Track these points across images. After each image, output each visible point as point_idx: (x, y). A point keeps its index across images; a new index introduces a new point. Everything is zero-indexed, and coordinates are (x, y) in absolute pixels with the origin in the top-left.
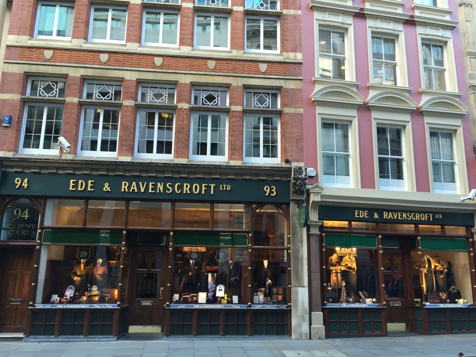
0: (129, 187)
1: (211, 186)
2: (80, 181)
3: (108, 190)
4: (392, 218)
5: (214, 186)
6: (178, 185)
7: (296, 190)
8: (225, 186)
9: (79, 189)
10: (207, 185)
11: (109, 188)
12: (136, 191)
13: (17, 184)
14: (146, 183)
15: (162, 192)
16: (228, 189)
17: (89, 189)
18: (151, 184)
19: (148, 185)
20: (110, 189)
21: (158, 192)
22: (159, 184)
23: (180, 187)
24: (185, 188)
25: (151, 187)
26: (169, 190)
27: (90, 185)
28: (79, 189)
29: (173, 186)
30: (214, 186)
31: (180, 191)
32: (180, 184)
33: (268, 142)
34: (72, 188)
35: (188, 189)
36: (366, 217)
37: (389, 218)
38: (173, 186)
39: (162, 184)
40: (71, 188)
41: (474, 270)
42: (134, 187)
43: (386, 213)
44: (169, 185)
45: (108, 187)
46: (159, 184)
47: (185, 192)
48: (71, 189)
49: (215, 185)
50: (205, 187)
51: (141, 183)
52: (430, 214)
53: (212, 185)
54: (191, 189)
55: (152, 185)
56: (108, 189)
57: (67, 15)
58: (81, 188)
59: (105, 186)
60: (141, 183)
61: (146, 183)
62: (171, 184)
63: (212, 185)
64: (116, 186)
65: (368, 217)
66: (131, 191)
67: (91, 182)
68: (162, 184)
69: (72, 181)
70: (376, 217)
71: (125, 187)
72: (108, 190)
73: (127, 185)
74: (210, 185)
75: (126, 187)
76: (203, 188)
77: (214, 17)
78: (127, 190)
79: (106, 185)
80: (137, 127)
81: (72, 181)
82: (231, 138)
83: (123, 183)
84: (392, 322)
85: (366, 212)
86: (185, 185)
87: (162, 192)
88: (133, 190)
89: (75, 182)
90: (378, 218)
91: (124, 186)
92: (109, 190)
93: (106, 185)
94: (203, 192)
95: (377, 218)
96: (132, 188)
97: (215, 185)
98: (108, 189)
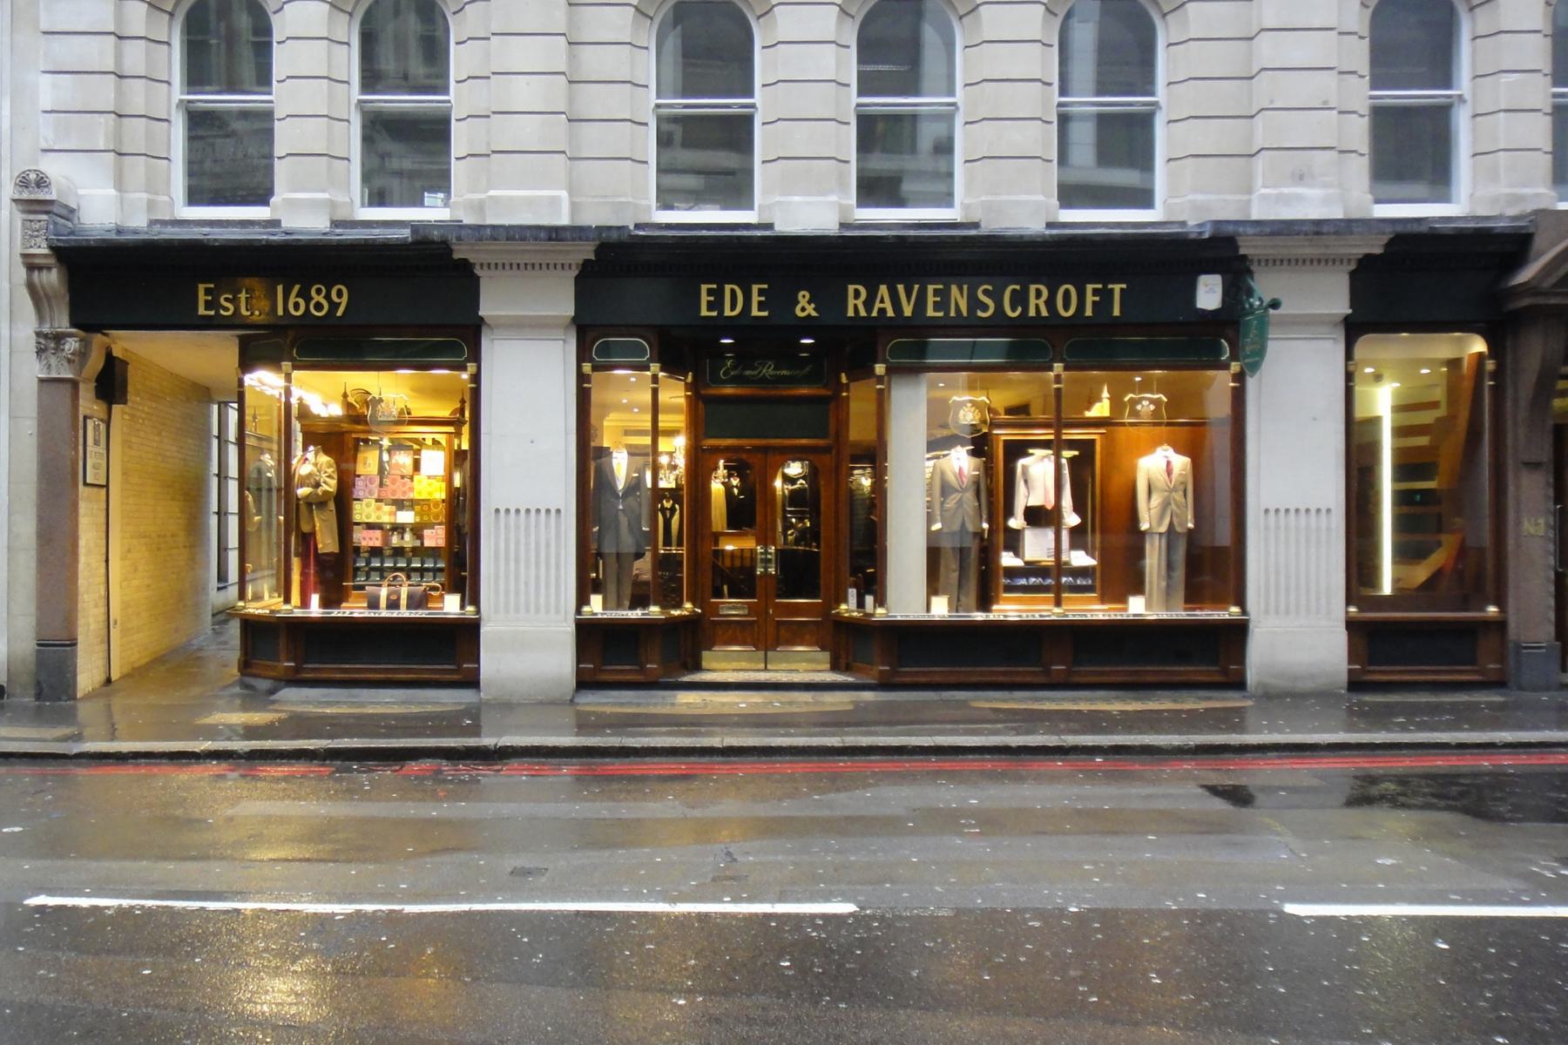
0: (869, 304)
2: (728, 288)
4: (890, 313)
5: (1122, 290)
6: (1014, 291)
9: (728, 313)
10: (1100, 286)
11: (813, 306)
13: (297, 296)
14: (916, 287)
15: (965, 313)
18: (931, 288)
20: (814, 309)
22: (954, 289)
23: (1020, 299)
24: (1033, 301)
25: (931, 299)
26: (985, 308)
27: (756, 299)
28: (728, 313)
29: (997, 297)
30: (1122, 290)
31: (1020, 309)
32: (1018, 287)
34: (759, 310)
36: (755, 312)
37: (874, 314)
38: (997, 297)
39: (965, 287)
40: (704, 312)
41: (844, 394)
42: (882, 301)
43: (1042, 287)
44: (986, 292)
46: (954, 289)
47: (1032, 313)
49: (1124, 286)
50: (1095, 292)
51: (900, 287)
53: (1117, 288)
54: (1050, 303)
55: (936, 292)
56: (811, 310)
57: (1349, 355)
58: (733, 308)
60: (900, 287)
61: (916, 287)
62: (990, 288)
63: (1117, 288)
64: (830, 299)
65: (765, 314)
66: (874, 314)
67: (760, 290)
68: (965, 287)
69: (704, 287)
70: (803, 309)
74: (1110, 286)
75: (860, 303)
76: (1090, 298)
77: (630, 454)
78: (863, 313)
80: (401, 740)
81: (704, 287)
83: (851, 288)
85: (935, 290)
86: (1033, 288)
87: (965, 313)
88: (882, 311)
89: (714, 289)
90: (814, 314)
91: (855, 303)
94: (1089, 312)
95: (809, 315)
96: (878, 305)
97: (1124, 286)
98: (811, 310)
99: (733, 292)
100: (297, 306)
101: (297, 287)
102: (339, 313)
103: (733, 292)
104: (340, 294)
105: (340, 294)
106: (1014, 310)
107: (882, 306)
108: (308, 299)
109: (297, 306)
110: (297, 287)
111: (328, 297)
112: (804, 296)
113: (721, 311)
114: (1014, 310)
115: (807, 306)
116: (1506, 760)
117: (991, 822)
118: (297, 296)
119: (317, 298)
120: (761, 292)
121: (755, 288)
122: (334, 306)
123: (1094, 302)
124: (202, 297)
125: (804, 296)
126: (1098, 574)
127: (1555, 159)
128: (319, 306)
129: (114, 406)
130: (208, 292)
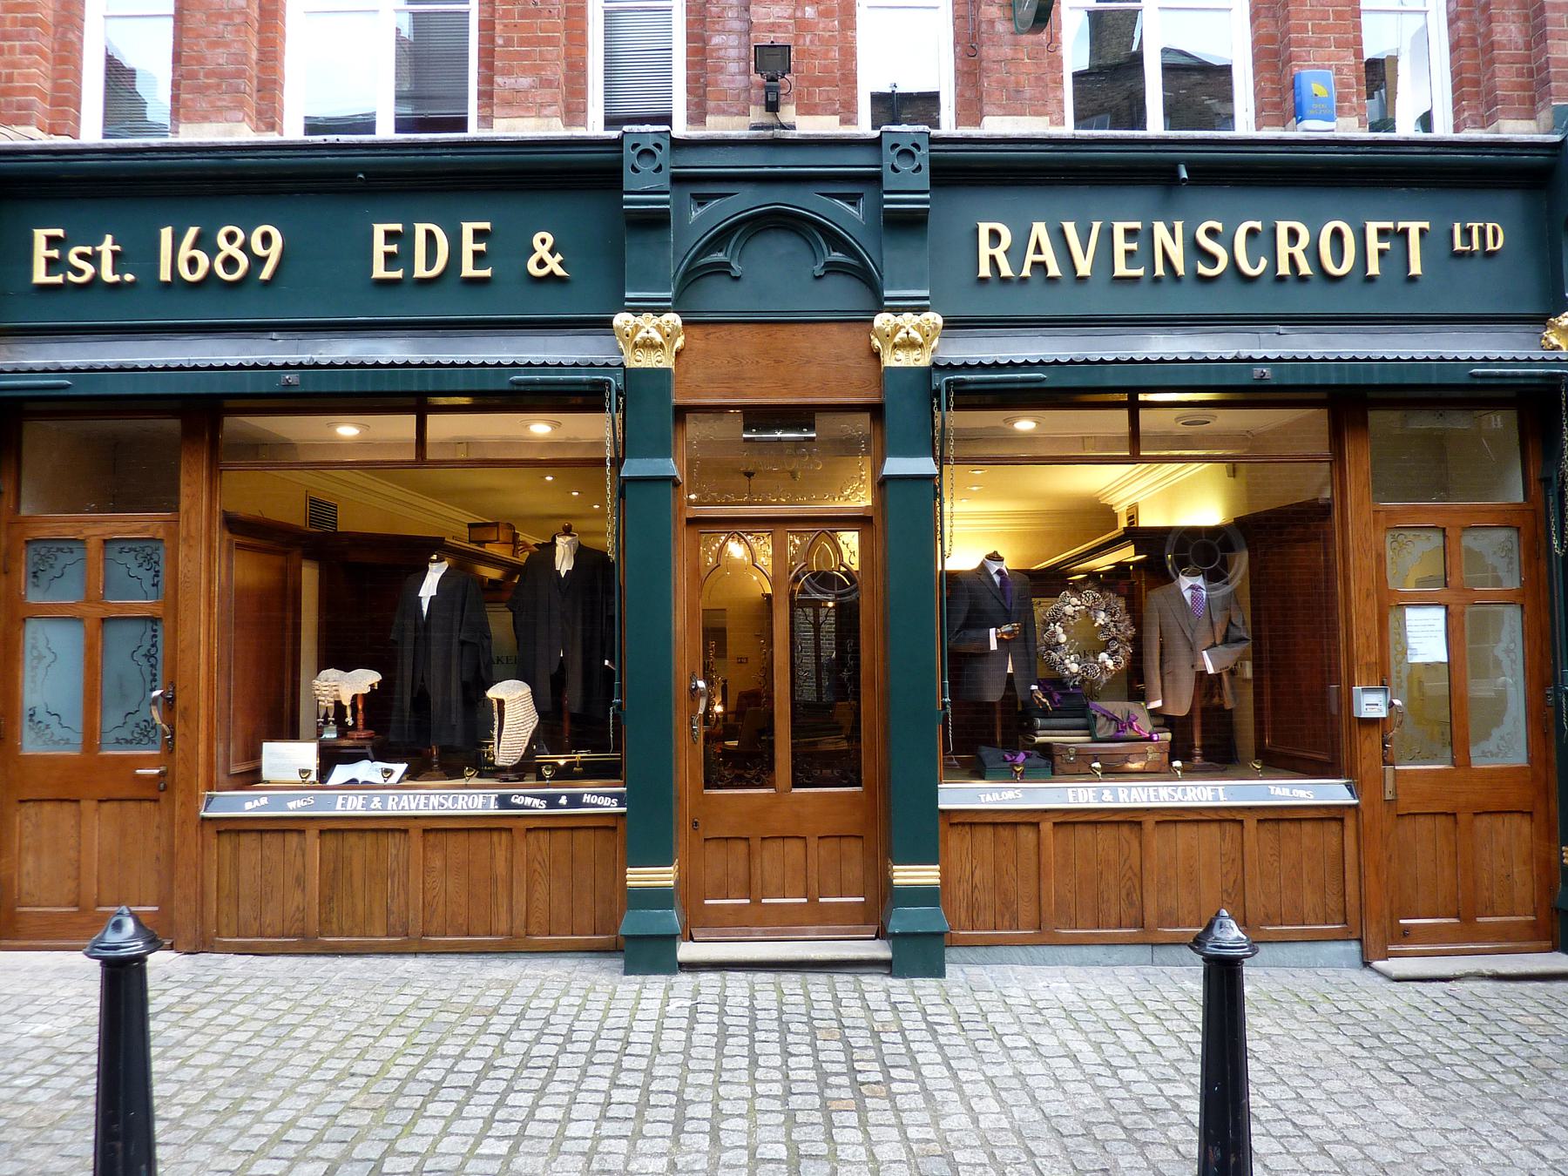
0: (1017, 255)
1: (1471, 227)
2: (420, 229)
3: (552, 272)
7: (1396, 229)
8: (1476, 226)
9: (420, 271)
11: (559, 257)
12: (1054, 270)
13: (195, 246)
14: (1096, 226)
16: (1490, 247)
17: (468, 270)
18: (1119, 228)
19: (1107, 235)
20: (560, 264)
21: (1160, 270)
23: (1262, 241)
25: (1121, 245)
27: (469, 246)
30: (1422, 231)
31: (1263, 262)
33: (779, 27)
35: (1298, 251)
42: (1038, 250)
45: (552, 252)
46: (1160, 229)
48: (379, 271)
49: (1426, 225)
51: (1070, 228)
52: (117, 278)
56: (554, 265)
58: (430, 264)
59: (220, 250)
61: (1096, 226)
63: (1414, 228)
68: (1179, 226)
70: (541, 264)
71: (995, 252)
72: (552, 272)
73: (1006, 238)
74: (1469, 225)
78: (1006, 271)
79: (543, 243)
81: (379, 230)
82: (956, 7)
83: (984, 229)
84: (989, 646)
88: (1040, 267)
92: (560, 272)
93: (543, 243)
96: (1031, 257)
97: (1426, 225)
98: (554, 265)
99: (430, 236)
100: (193, 263)
101: (192, 232)
102: (266, 274)
103: (430, 236)
104: (266, 239)
105: (266, 239)
106: (1255, 265)
107: (1038, 258)
108: (213, 251)
109: (193, 263)
110: (192, 232)
111: (246, 248)
112: (543, 241)
113: (410, 266)
114: (1255, 265)
115: (548, 258)
116: (141, 607)
117: (230, 667)
118: (195, 246)
119: (228, 249)
120: (479, 235)
121: (468, 228)
122: (258, 262)
123: (1382, 253)
124: (41, 252)
125: (543, 241)
126: (877, 521)
127: (175, 22)
128: (230, 263)
129: (1512, 415)
130: (52, 242)
